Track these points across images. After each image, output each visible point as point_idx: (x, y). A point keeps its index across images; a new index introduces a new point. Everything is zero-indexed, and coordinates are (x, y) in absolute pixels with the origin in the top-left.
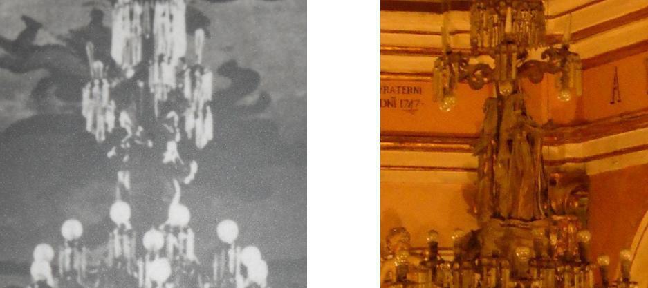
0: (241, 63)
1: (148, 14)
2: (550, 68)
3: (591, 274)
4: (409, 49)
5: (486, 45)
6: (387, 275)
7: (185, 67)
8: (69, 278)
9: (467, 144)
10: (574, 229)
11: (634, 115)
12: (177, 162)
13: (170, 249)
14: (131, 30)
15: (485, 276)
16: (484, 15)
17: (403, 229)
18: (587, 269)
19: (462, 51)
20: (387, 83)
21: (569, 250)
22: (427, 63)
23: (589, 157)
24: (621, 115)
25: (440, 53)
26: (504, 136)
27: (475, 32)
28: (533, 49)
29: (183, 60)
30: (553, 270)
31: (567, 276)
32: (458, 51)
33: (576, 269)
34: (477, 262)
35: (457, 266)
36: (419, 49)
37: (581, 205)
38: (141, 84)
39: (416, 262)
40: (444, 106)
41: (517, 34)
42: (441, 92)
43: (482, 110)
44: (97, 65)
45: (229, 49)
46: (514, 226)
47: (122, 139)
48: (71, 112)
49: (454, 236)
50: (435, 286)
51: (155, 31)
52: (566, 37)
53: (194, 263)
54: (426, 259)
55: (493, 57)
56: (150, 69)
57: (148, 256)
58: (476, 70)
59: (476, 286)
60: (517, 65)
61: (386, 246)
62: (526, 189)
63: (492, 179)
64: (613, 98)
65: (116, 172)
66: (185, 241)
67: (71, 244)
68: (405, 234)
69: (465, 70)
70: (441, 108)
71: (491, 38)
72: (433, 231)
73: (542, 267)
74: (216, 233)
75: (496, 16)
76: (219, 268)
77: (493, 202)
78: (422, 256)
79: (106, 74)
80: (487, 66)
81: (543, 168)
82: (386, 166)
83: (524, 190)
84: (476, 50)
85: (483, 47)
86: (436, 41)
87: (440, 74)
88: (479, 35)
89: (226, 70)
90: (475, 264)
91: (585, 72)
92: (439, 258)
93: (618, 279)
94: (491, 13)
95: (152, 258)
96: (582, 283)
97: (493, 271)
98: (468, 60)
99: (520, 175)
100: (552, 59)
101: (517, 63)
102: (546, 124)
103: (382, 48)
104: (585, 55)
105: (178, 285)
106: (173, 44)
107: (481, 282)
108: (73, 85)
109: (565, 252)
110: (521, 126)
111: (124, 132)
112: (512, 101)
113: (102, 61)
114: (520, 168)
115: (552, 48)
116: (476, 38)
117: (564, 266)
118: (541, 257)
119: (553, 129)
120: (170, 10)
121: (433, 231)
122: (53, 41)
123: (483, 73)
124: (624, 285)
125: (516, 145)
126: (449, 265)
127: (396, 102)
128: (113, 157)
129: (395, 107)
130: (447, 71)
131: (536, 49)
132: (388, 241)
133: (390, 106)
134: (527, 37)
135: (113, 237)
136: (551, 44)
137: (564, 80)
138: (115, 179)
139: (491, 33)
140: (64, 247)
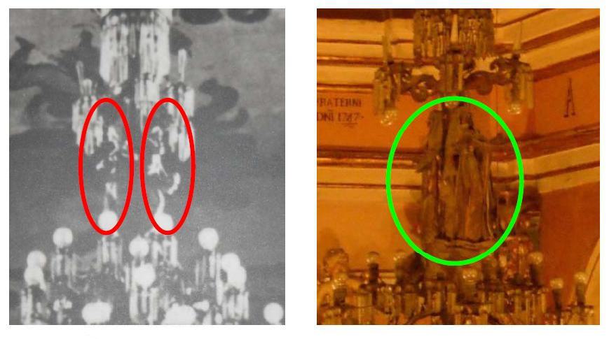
0: (222, 81)
1: (134, 35)
2: (500, 80)
3: (543, 298)
4: (347, 59)
5: (430, 54)
6: (324, 298)
7: (168, 85)
8: (60, 283)
9: (410, 159)
10: (525, 251)
11: (590, 129)
12: (162, 174)
13: (155, 256)
14: (118, 50)
15: (429, 300)
16: (429, 23)
17: (342, 251)
18: (539, 293)
19: (405, 61)
20: (324, 96)
21: (520, 272)
22: (367, 74)
23: (540, 174)
24: (576, 129)
25: (381, 63)
26: (450, 151)
27: (419, 41)
28: (481, 60)
29: (167, 78)
30: (503, 294)
31: (517, 300)
32: (400, 61)
33: (527, 293)
34: (420, 285)
35: (399, 289)
36: (359, 59)
37: (533, 225)
38: (127, 101)
39: (355, 285)
40: (385, 120)
41: (464, 43)
42: (382, 106)
43: (426, 125)
44: (87, 83)
45: (210, 68)
46: (460, 247)
47: (110, 152)
48: (61, 127)
49: (396, 257)
50: (375, 310)
51: (141, 51)
52: (517, 46)
53: (177, 268)
54: (366, 282)
55: (438, 67)
56: (136, 87)
57: (134, 263)
58: (420, 81)
59: (419, 310)
60: (463, 76)
61: (322, 267)
62: (473, 208)
63: (437, 198)
64: (567, 112)
65: (104, 183)
66: (169, 249)
67: (62, 251)
68: (343, 255)
69: (408, 82)
70: (382, 122)
71: (436, 47)
72: (373, 253)
73: (490, 290)
74: (197, 241)
75: (441, 25)
76: (201, 274)
77: (438, 220)
78: (362, 278)
79: (95, 92)
80: (431, 77)
81: (492, 185)
82: (322, 184)
83: (471, 209)
84: (419, 61)
85: (427, 57)
86: (377, 51)
87: (381, 86)
88: (422, 44)
89: (207, 87)
90: (418, 287)
91: (539, 84)
92: (379, 281)
93: (573, 302)
94: (436, 22)
95: (138, 264)
96: (534, 308)
97: (438, 295)
98: (411, 71)
99: (466, 193)
100: (501, 69)
101: (463, 74)
102: (495, 139)
103: (319, 58)
104: (536, 66)
105: (162, 289)
106: (157, 64)
107: (424, 306)
108: (63, 101)
109: (516, 275)
110: (468, 141)
111: (111, 145)
112: (458, 116)
113: (91, 79)
114: (467, 185)
115: (501, 58)
116: (420, 47)
117: (515, 289)
118: (490, 280)
119: (502, 144)
120: (154, 32)
121: (373, 253)
122: (45, 60)
123: (426, 84)
124: (578, 309)
125: (462, 161)
126: (390, 289)
127: (334, 115)
128: (101, 169)
129: (333, 120)
130: (388, 83)
131: (484, 59)
132: (325, 263)
133: (327, 119)
134: (475, 47)
135: (102, 244)
136: (500, 53)
137: (514, 93)
138: (104, 189)
139: (436, 43)
140: (56, 254)
